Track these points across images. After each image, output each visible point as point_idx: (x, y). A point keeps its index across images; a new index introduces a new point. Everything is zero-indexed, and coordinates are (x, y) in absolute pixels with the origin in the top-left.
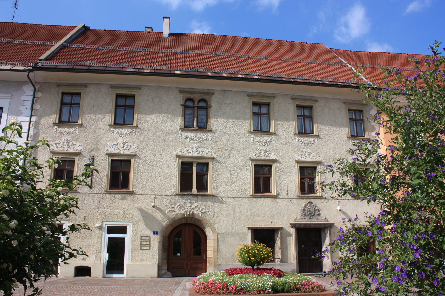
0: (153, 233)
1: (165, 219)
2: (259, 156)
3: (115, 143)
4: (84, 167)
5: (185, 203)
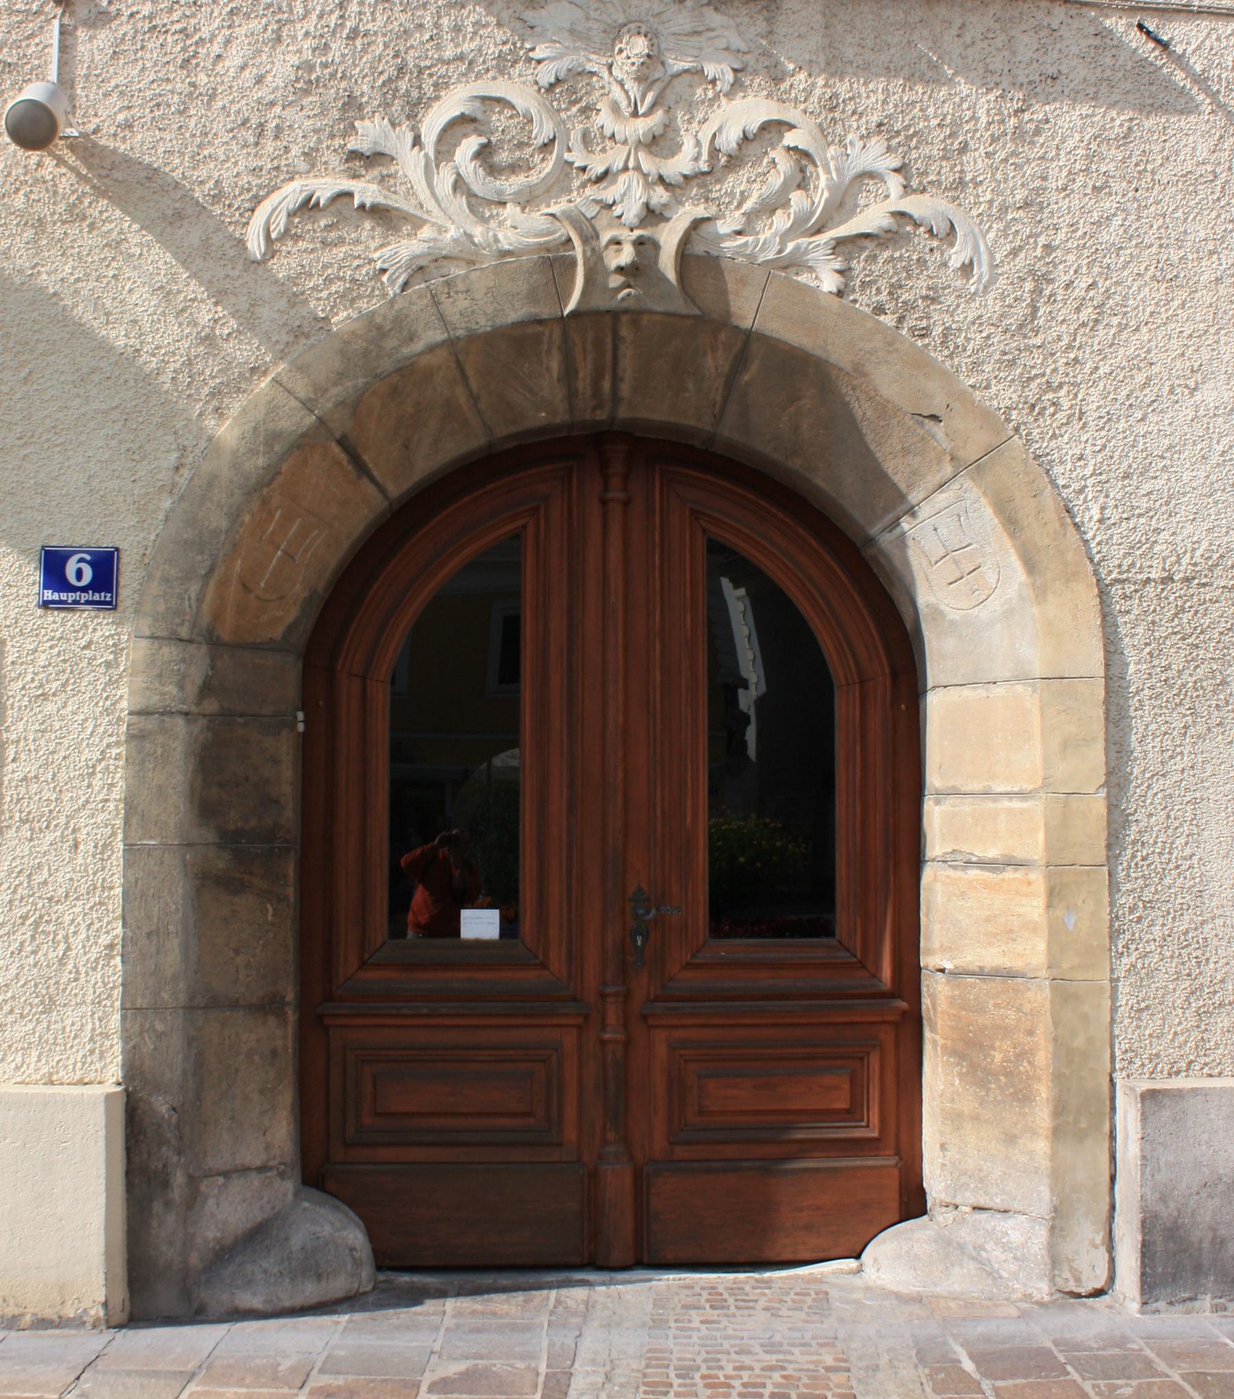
0: (34, 574)
1: (245, 351)
5: (567, 88)
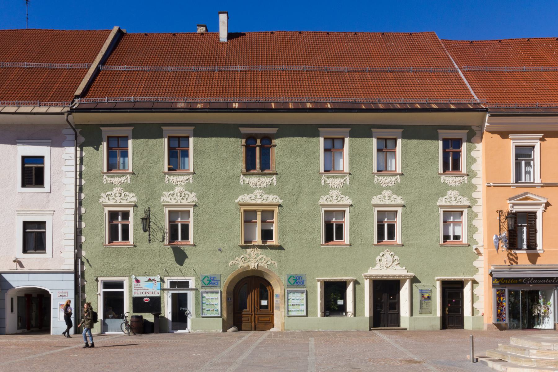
2: (330, 201)
3: (172, 192)
4: (141, 221)
